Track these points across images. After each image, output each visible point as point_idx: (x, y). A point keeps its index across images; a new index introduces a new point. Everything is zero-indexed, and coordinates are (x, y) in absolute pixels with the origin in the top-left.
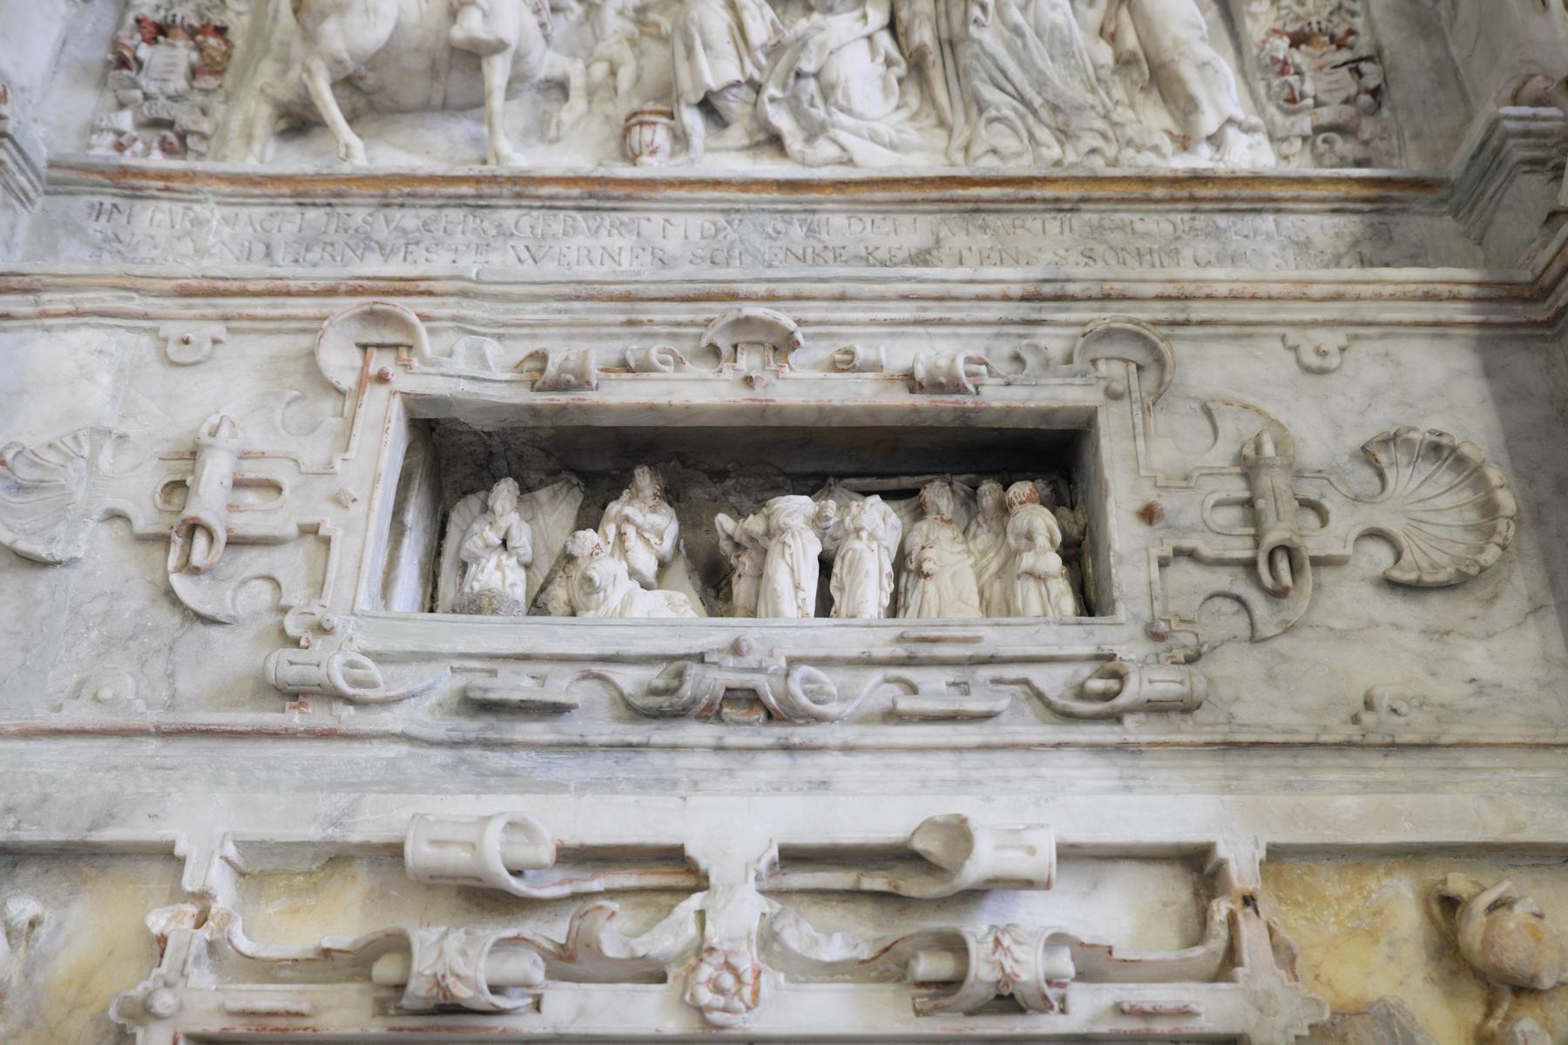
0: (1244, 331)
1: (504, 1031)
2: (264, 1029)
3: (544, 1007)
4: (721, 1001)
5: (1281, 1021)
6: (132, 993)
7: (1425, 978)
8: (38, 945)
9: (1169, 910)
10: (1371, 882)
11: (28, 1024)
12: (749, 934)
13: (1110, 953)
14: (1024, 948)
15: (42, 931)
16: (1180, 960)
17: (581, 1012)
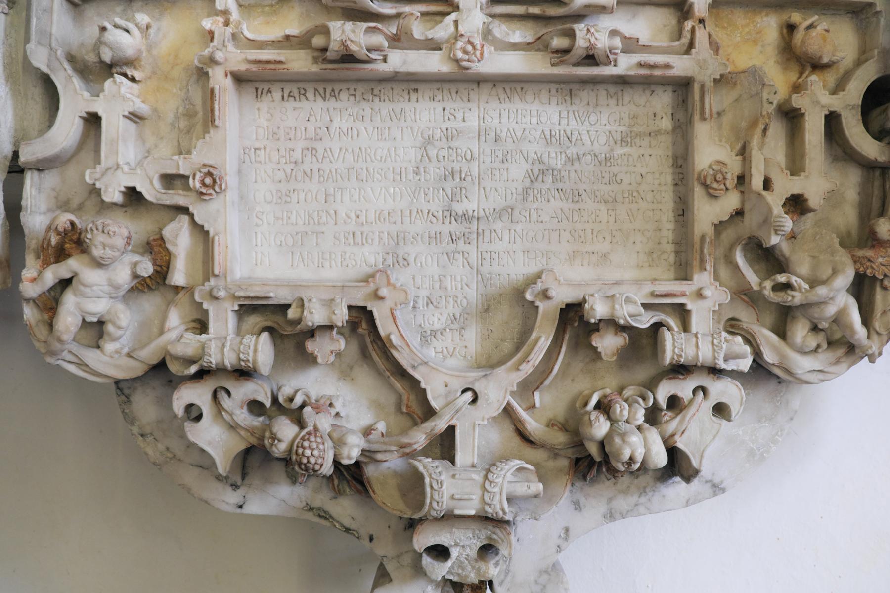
1: (372, 70)
2: (265, 69)
3: (389, 60)
4: (466, 57)
5: (709, 72)
6: (203, 53)
7: (775, 62)
8: (151, 38)
9: (666, 28)
10: (758, 19)
11: (154, 73)
12: (478, 30)
13: (638, 41)
14: (600, 33)
15: (152, 31)
16: (668, 47)
17: (405, 63)
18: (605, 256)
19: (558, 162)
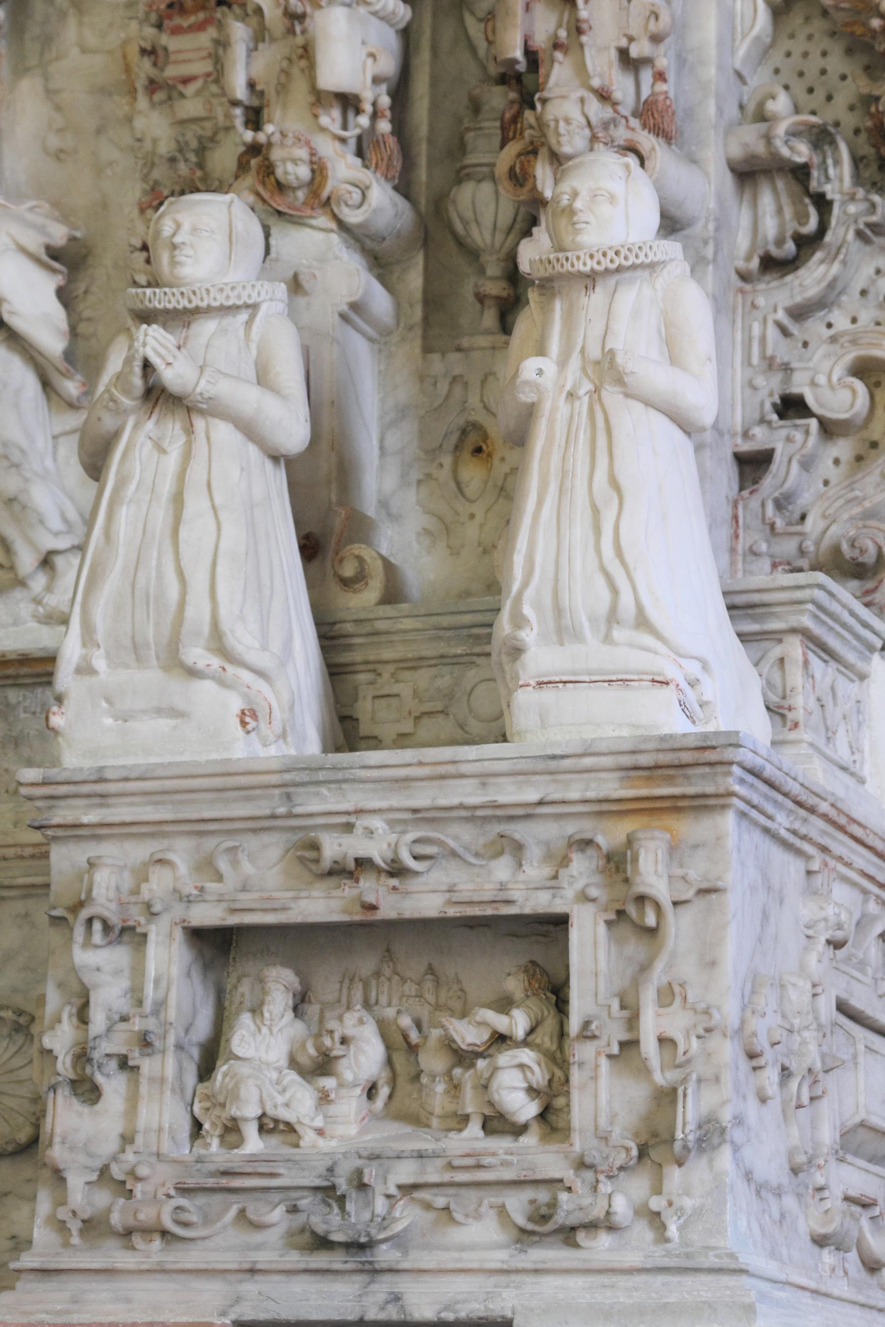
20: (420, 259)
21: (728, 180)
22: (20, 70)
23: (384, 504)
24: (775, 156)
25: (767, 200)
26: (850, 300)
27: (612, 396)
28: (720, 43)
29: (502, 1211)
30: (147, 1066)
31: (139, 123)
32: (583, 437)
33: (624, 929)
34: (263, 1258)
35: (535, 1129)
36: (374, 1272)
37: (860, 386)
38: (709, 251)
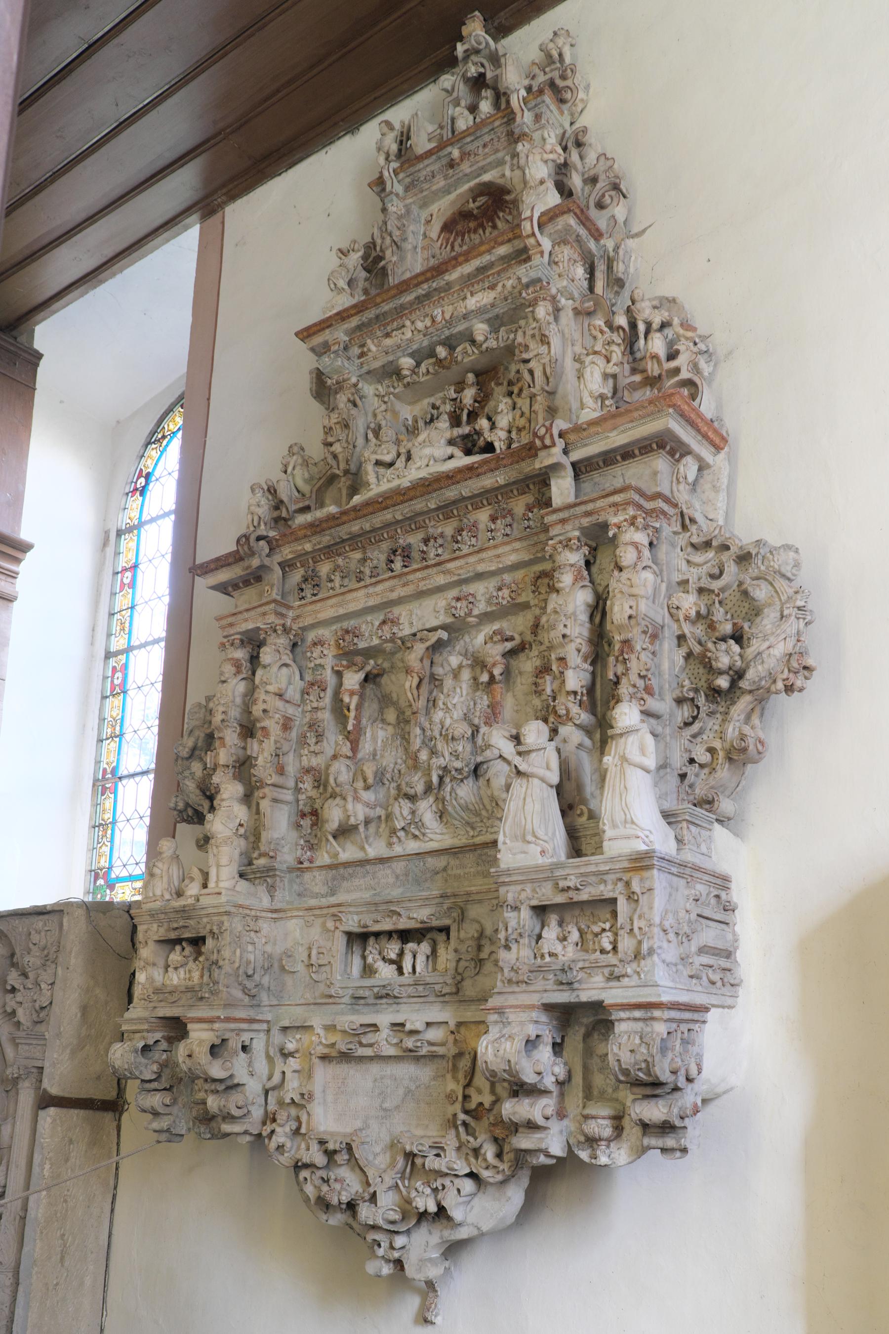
0: (480, 901)
15: (691, 344)
18: (427, 1126)
19: (413, 1088)
20: (599, 731)
21: (674, 704)
22: (507, 691)
23: (592, 794)
24: (684, 696)
25: (685, 708)
26: (708, 732)
27: (625, 765)
28: (670, 669)
29: (603, 973)
30: (521, 941)
31: (533, 702)
32: (618, 776)
33: (631, 901)
34: (548, 987)
35: (612, 952)
36: (574, 990)
37: (708, 754)
38: (668, 723)
